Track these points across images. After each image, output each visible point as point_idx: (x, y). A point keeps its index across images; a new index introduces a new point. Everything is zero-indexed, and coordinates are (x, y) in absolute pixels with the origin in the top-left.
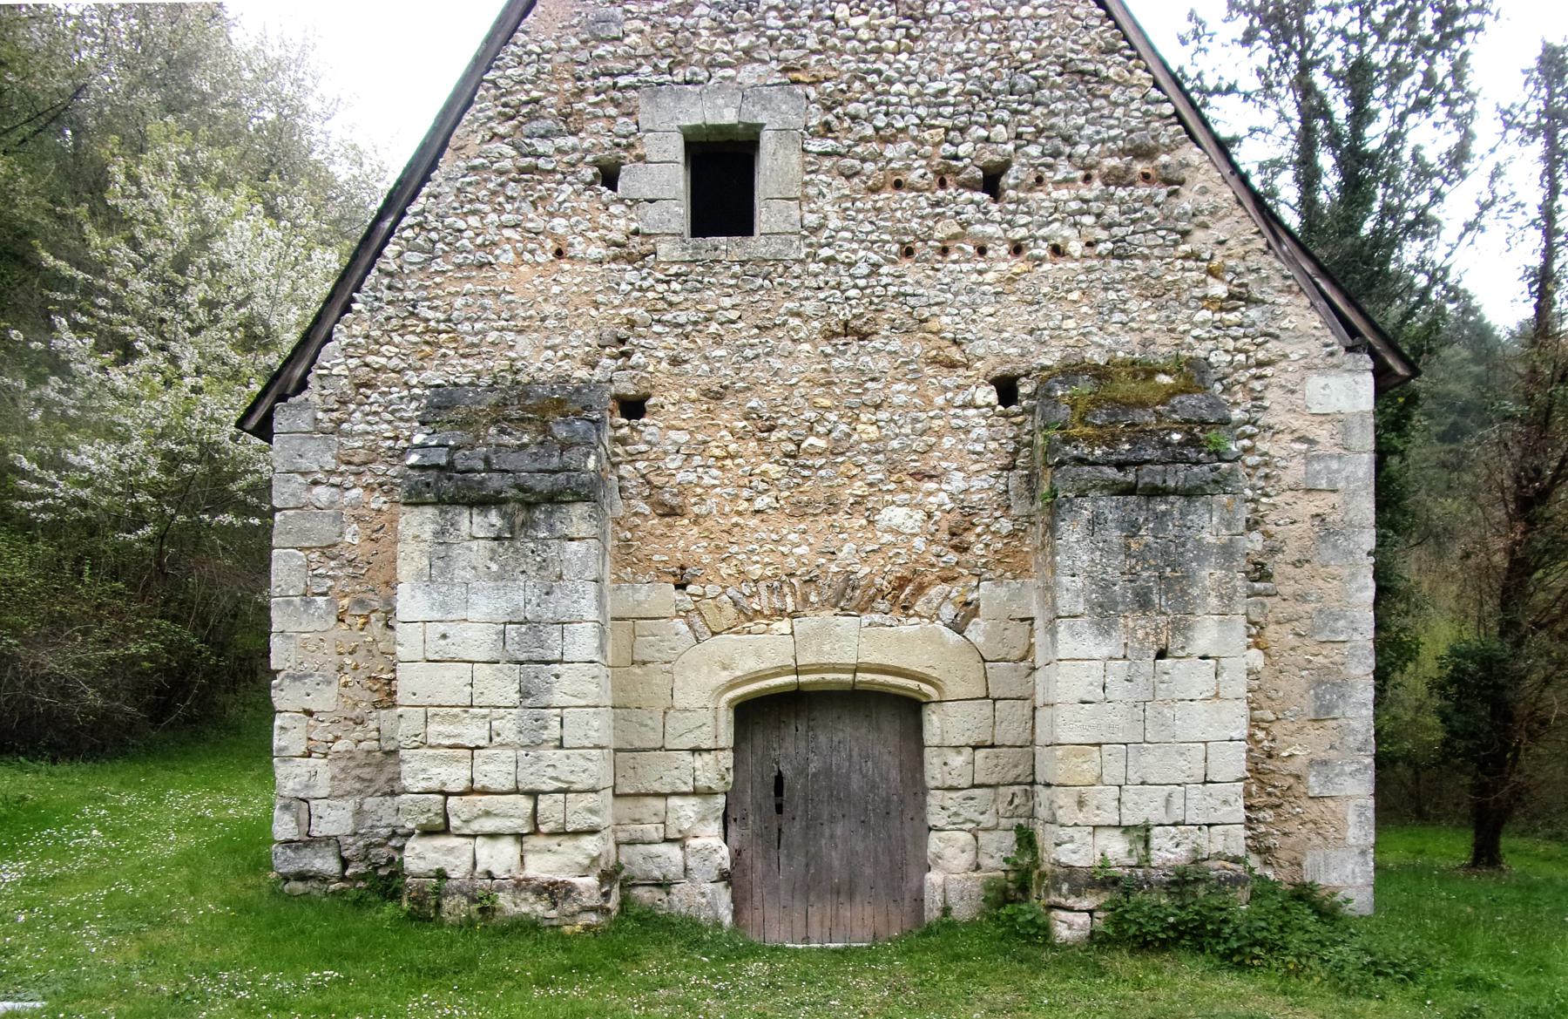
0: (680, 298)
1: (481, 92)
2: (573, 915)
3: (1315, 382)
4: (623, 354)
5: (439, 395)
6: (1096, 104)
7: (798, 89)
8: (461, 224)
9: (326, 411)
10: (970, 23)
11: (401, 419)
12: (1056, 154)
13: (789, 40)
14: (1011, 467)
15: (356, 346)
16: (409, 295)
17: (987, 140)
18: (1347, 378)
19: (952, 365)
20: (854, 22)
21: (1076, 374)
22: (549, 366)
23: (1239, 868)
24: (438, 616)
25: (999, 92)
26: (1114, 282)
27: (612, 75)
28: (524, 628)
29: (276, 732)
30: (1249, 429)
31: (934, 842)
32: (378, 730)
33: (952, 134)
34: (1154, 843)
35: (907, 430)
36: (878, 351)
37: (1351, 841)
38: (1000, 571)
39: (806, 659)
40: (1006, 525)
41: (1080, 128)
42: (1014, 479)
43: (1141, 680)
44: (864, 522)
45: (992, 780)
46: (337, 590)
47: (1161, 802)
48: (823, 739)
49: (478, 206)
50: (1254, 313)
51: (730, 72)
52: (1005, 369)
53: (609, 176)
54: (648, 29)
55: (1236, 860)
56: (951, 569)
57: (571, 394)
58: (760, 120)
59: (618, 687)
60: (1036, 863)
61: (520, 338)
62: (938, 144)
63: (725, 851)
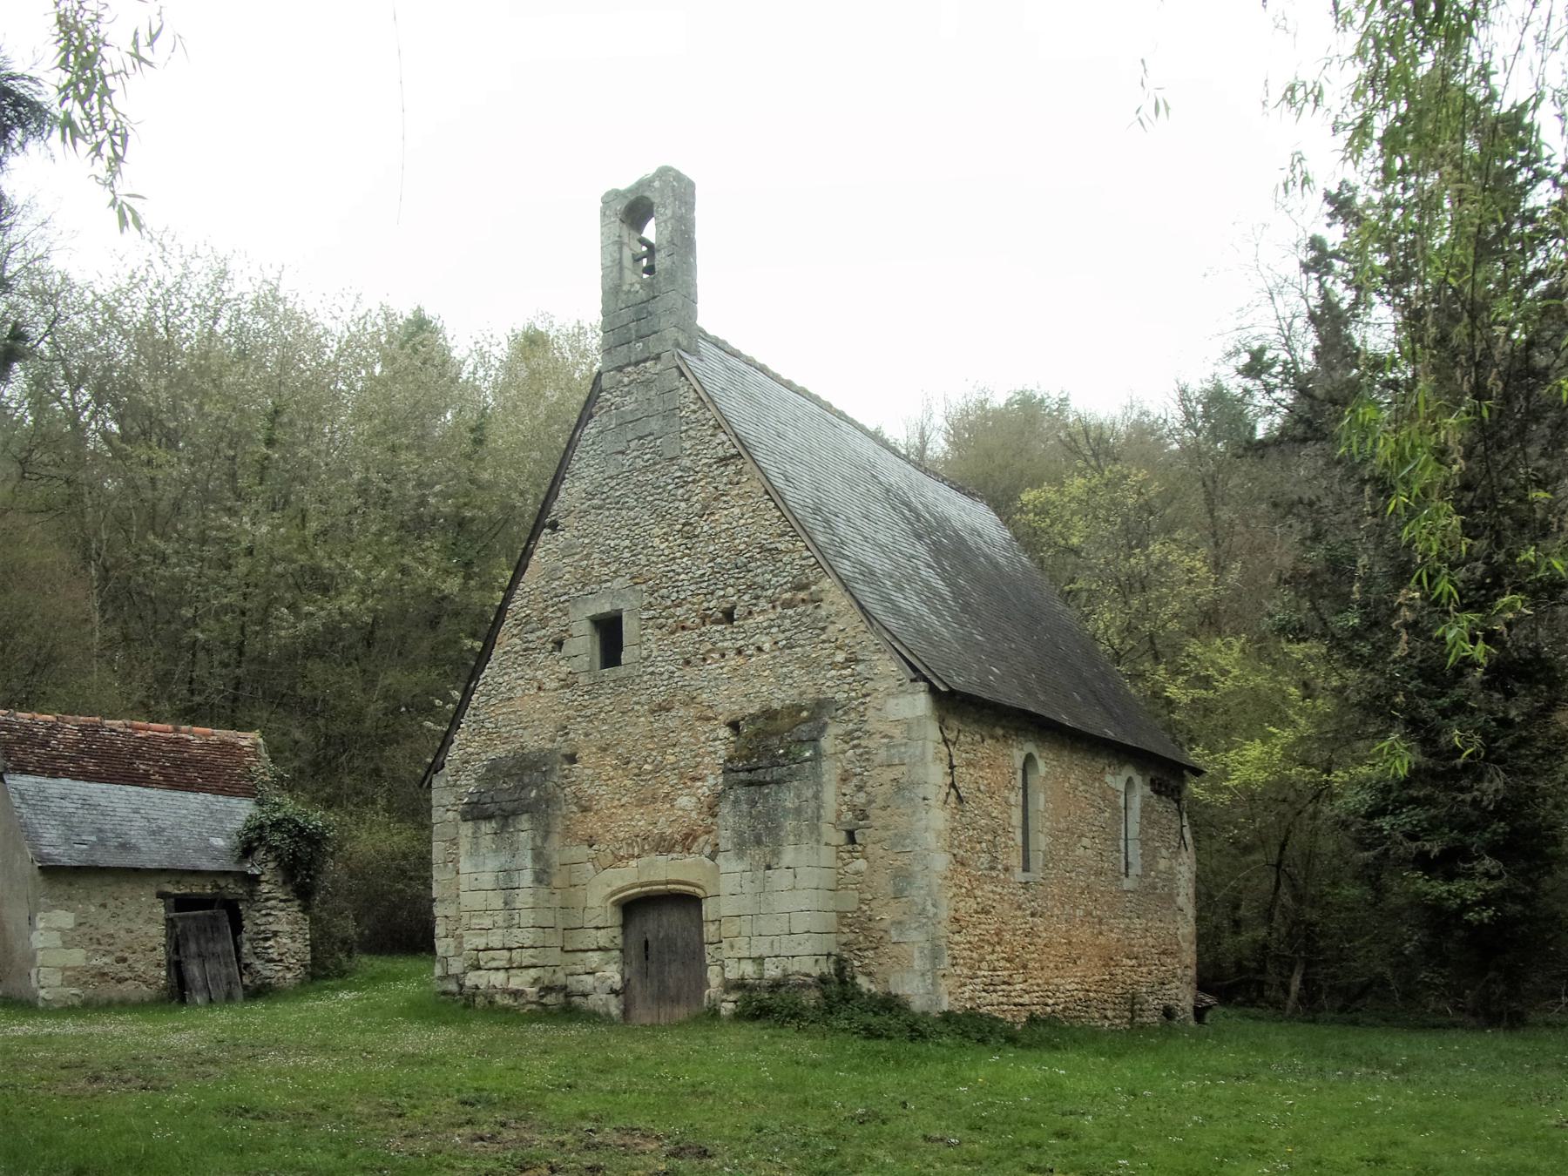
3: (892, 702)
7: (638, 587)
8: (501, 680)
17: (723, 596)
18: (909, 697)
19: (708, 719)
20: (662, 547)
37: (916, 968)
39: (644, 879)
41: (769, 581)
47: (768, 945)
48: (664, 919)
50: (860, 668)
53: (559, 644)
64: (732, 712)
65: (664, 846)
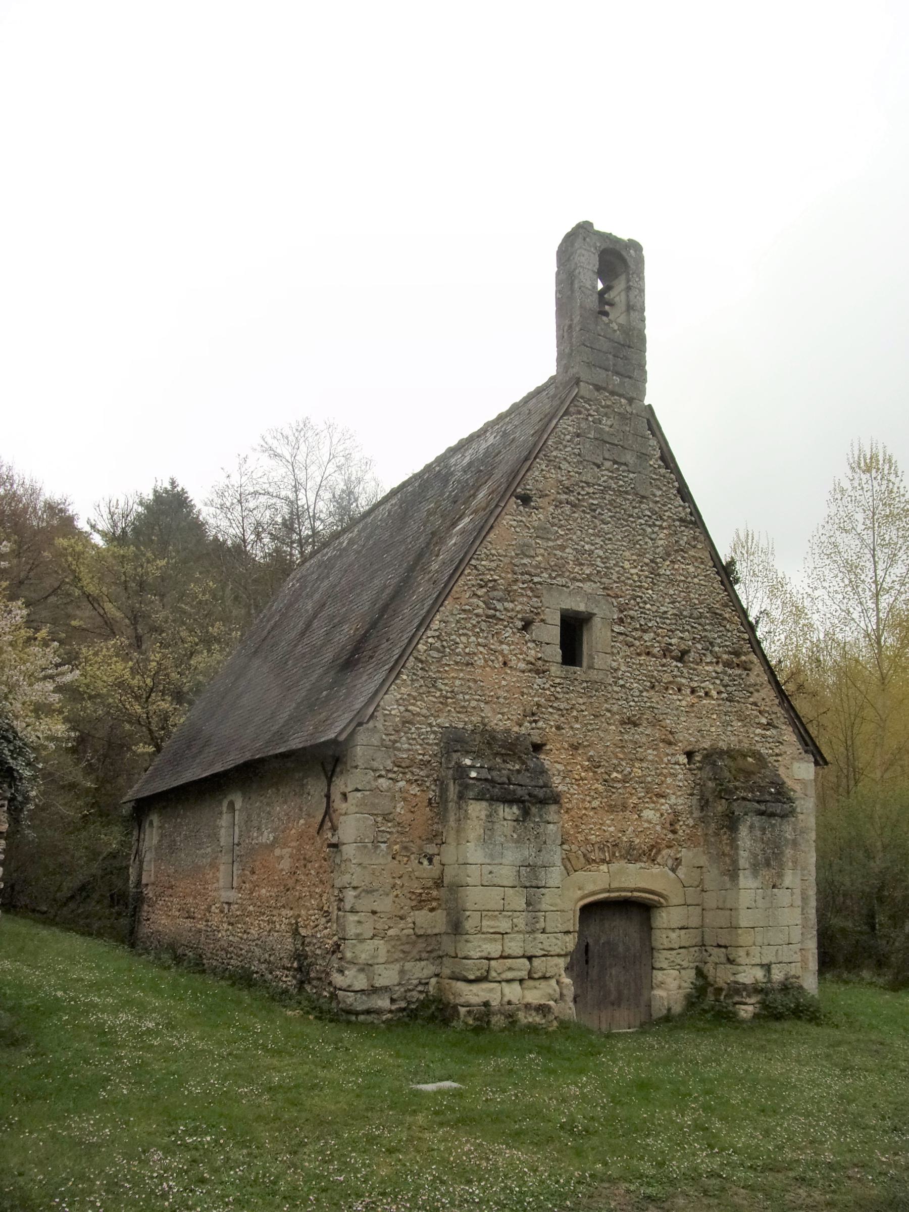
3: (796, 765)
9: (387, 735)
11: (427, 744)
15: (404, 700)
19: (670, 743)
22: (501, 724)
24: (488, 861)
25: (686, 617)
28: (528, 870)
31: (658, 976)
32: (414, 923)
34: (773, 971)
36: (642, 733)
39: (615, 885)
45: (686, 945)
46: (392, 840)
48: (607, 925)
51: (581, 585)
52: (689, 748)
53: (527, 625)
58: (595, 611)
61: (486, 706)
64: (690, 743)
65: (632, 854)
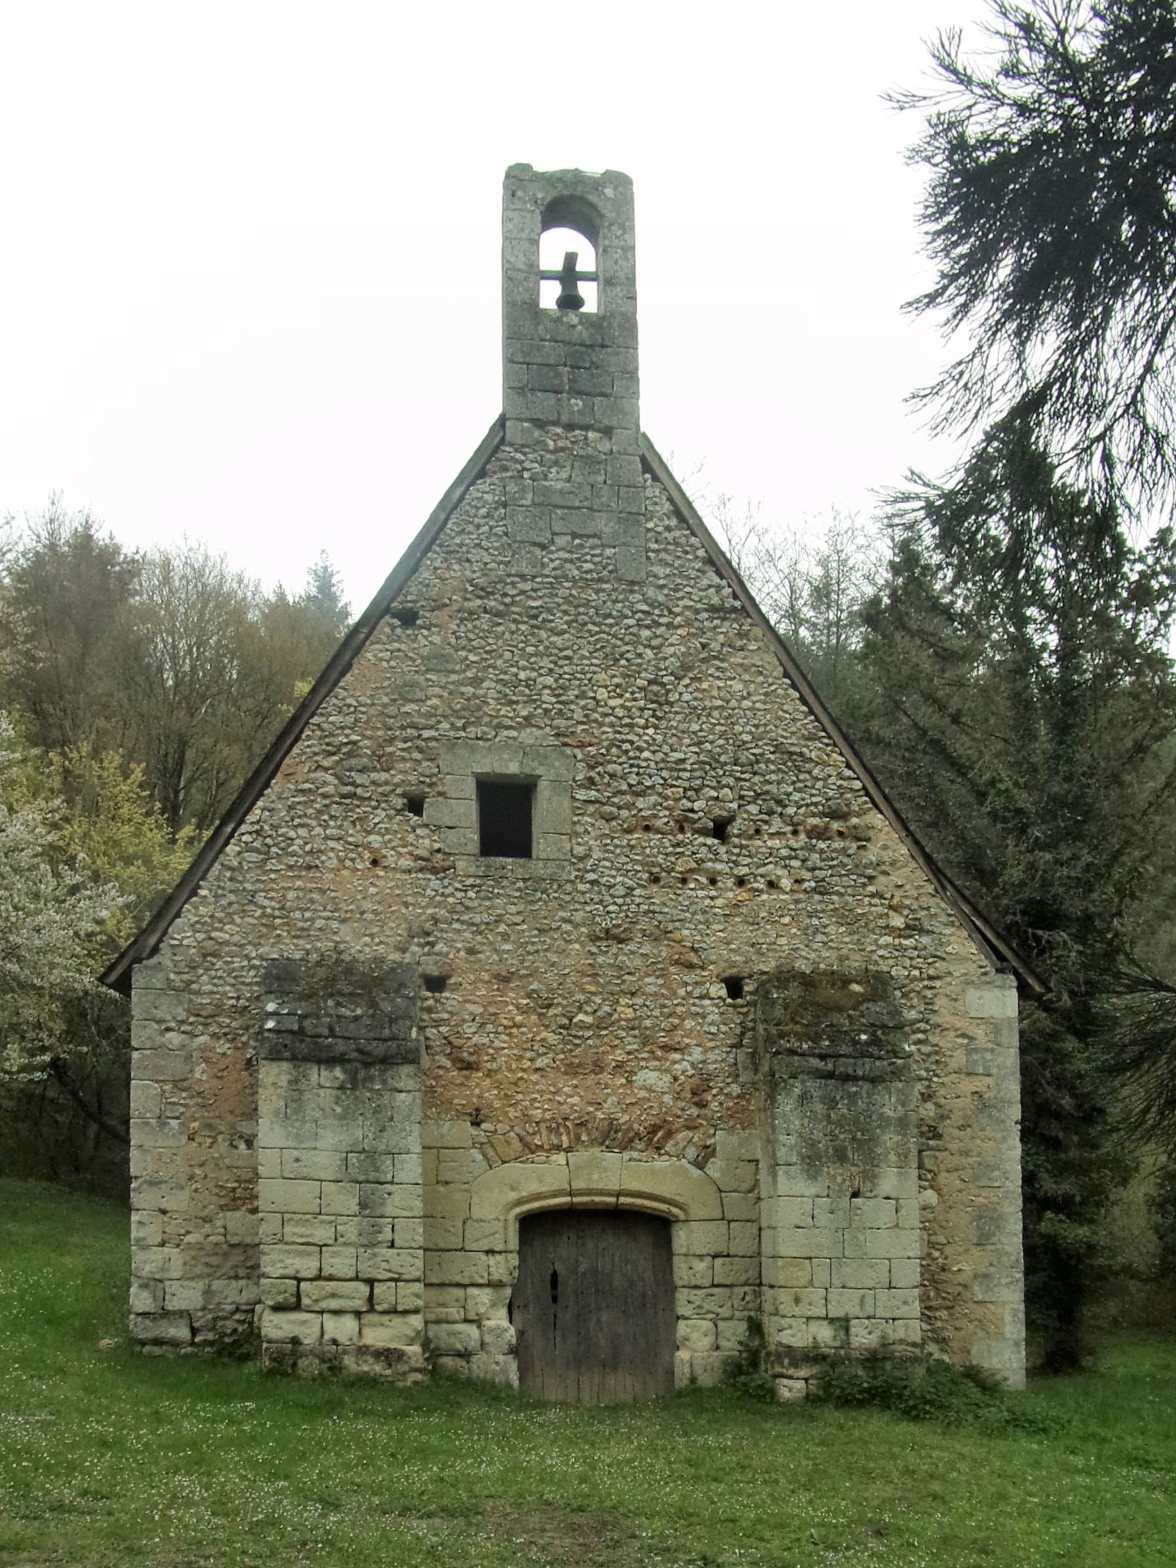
0: (476, 903)
1: (307, 732)
2: (404, 1374)
3: (972, 995)
4: (428, 943)
5: (277, 967)
6: (801, 777)
7: (568, 751)
8: (292, 834)
10: (703, 709)
12: (771, 813)
13: (560, 713)
14: (738, 1045)
16: (248, 886)
17: (717, 798)
18: (997, 992)
19: (691, 966)
20: (612, 703)
21: (787, 980)
22: (367, 950)
23: (917, 1351)
24: (293, 1144)
25: (726, 764)
26: (816, 911)
27: (417, 728)
29: (133, 1226)
30: (922, 1026)
31: (682, 1328)
33: (689, 793)
34: (853, 1331)
35: (657, 1013)
36: (632, 953)
37: (1008, 1335)
38: (731, 1123)
39: (579, 1184)
40: (736, 1089)
41: (790, 794)
42: (741, 1055)
43: (841, 1213)
44: (624, 1081)
45: (728, 1281)
46: (188, 1115)
47: (857, 1301)
48: (590, 1245)
49: (306, 820)
50: (925, 940)
51: (514, 733)
53: (415, 805)
54: (445, 694)
55: (914, 1345)
56: (693, 1120)
57: (387, 973)
58: (538, 772)
59: (426, 1202)
60: (763, 1345)
62: (677, 800)
63: (512, 1331)
